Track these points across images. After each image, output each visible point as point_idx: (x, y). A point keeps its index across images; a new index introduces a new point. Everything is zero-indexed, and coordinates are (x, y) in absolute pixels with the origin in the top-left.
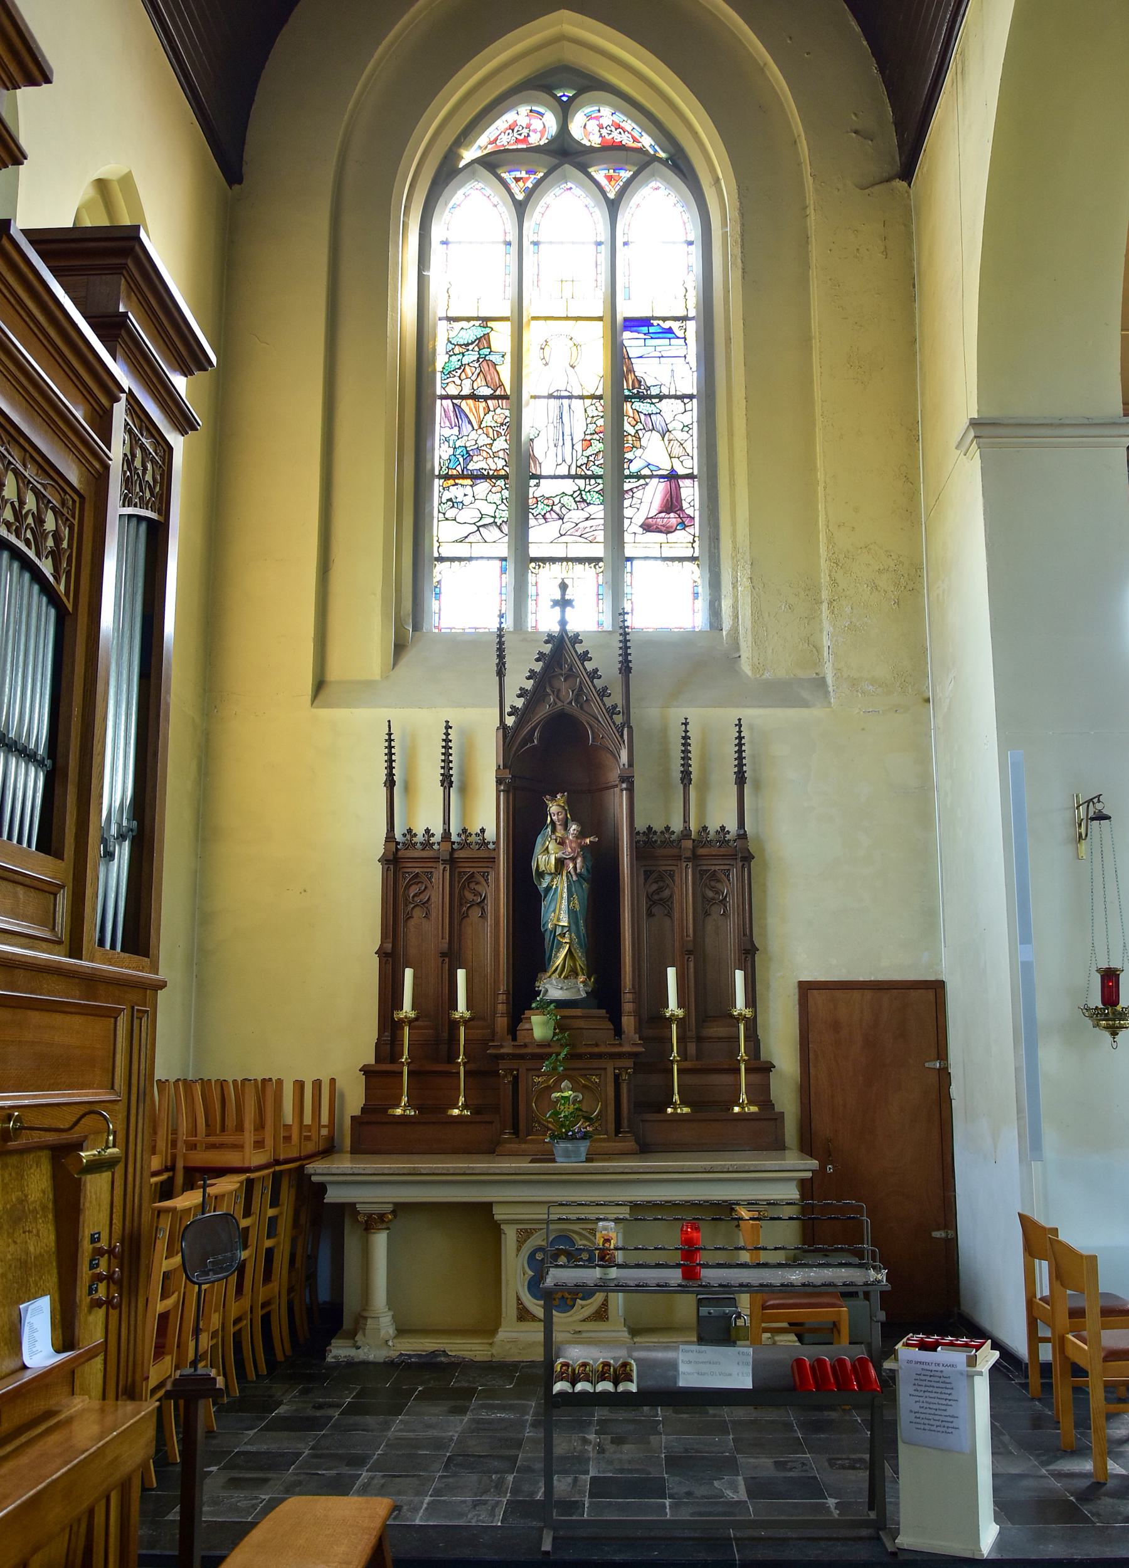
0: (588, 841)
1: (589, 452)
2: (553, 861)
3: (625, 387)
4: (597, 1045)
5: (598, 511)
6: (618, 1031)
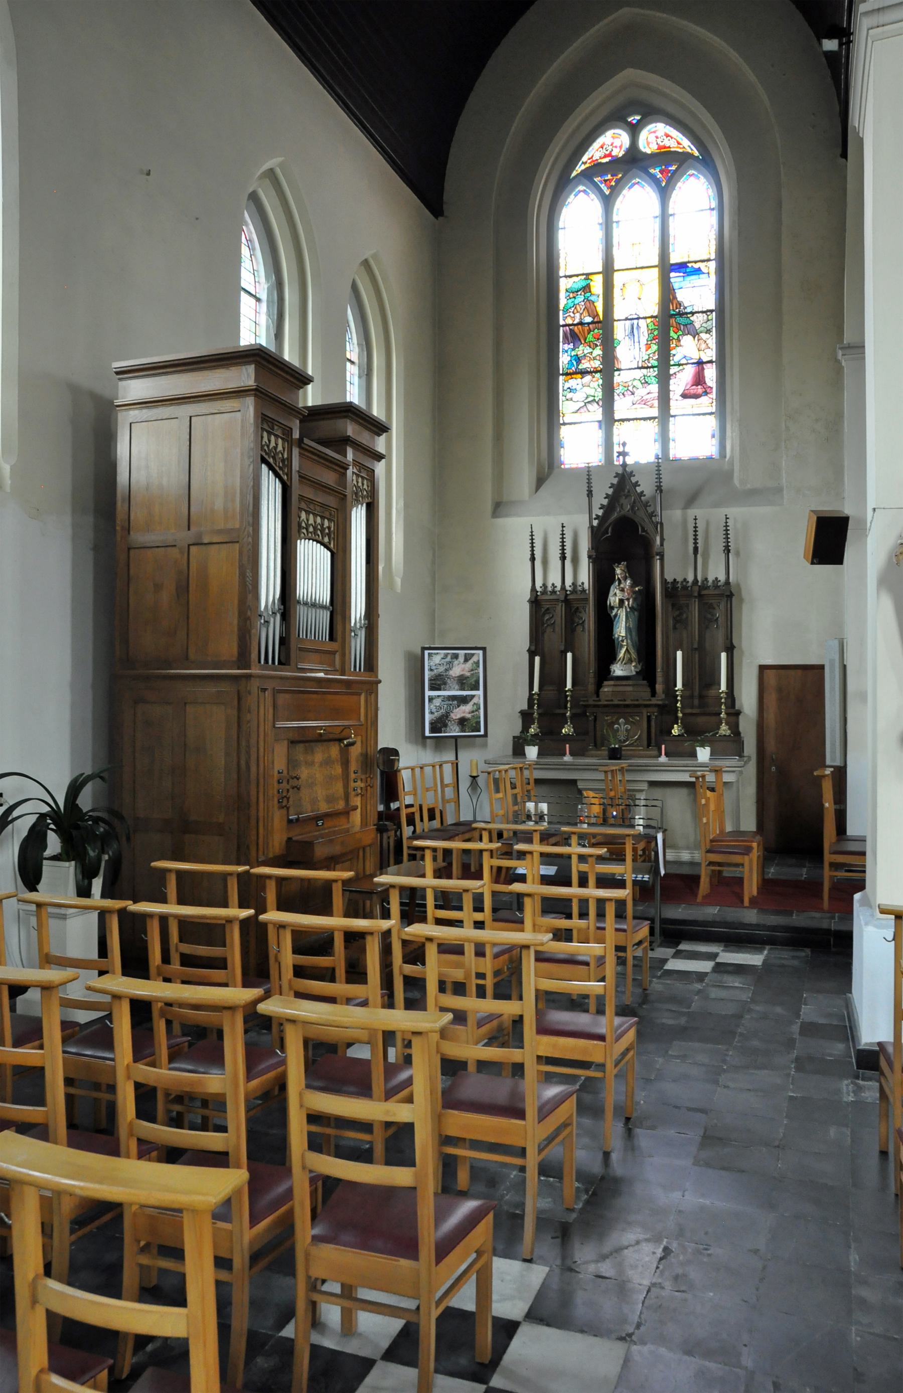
0: (637, 589)
1: (650, 351)
2: (617, 601)
3: (671, 308)
4: (625, 700)
5: (654, 388)
6: (654, 693)
